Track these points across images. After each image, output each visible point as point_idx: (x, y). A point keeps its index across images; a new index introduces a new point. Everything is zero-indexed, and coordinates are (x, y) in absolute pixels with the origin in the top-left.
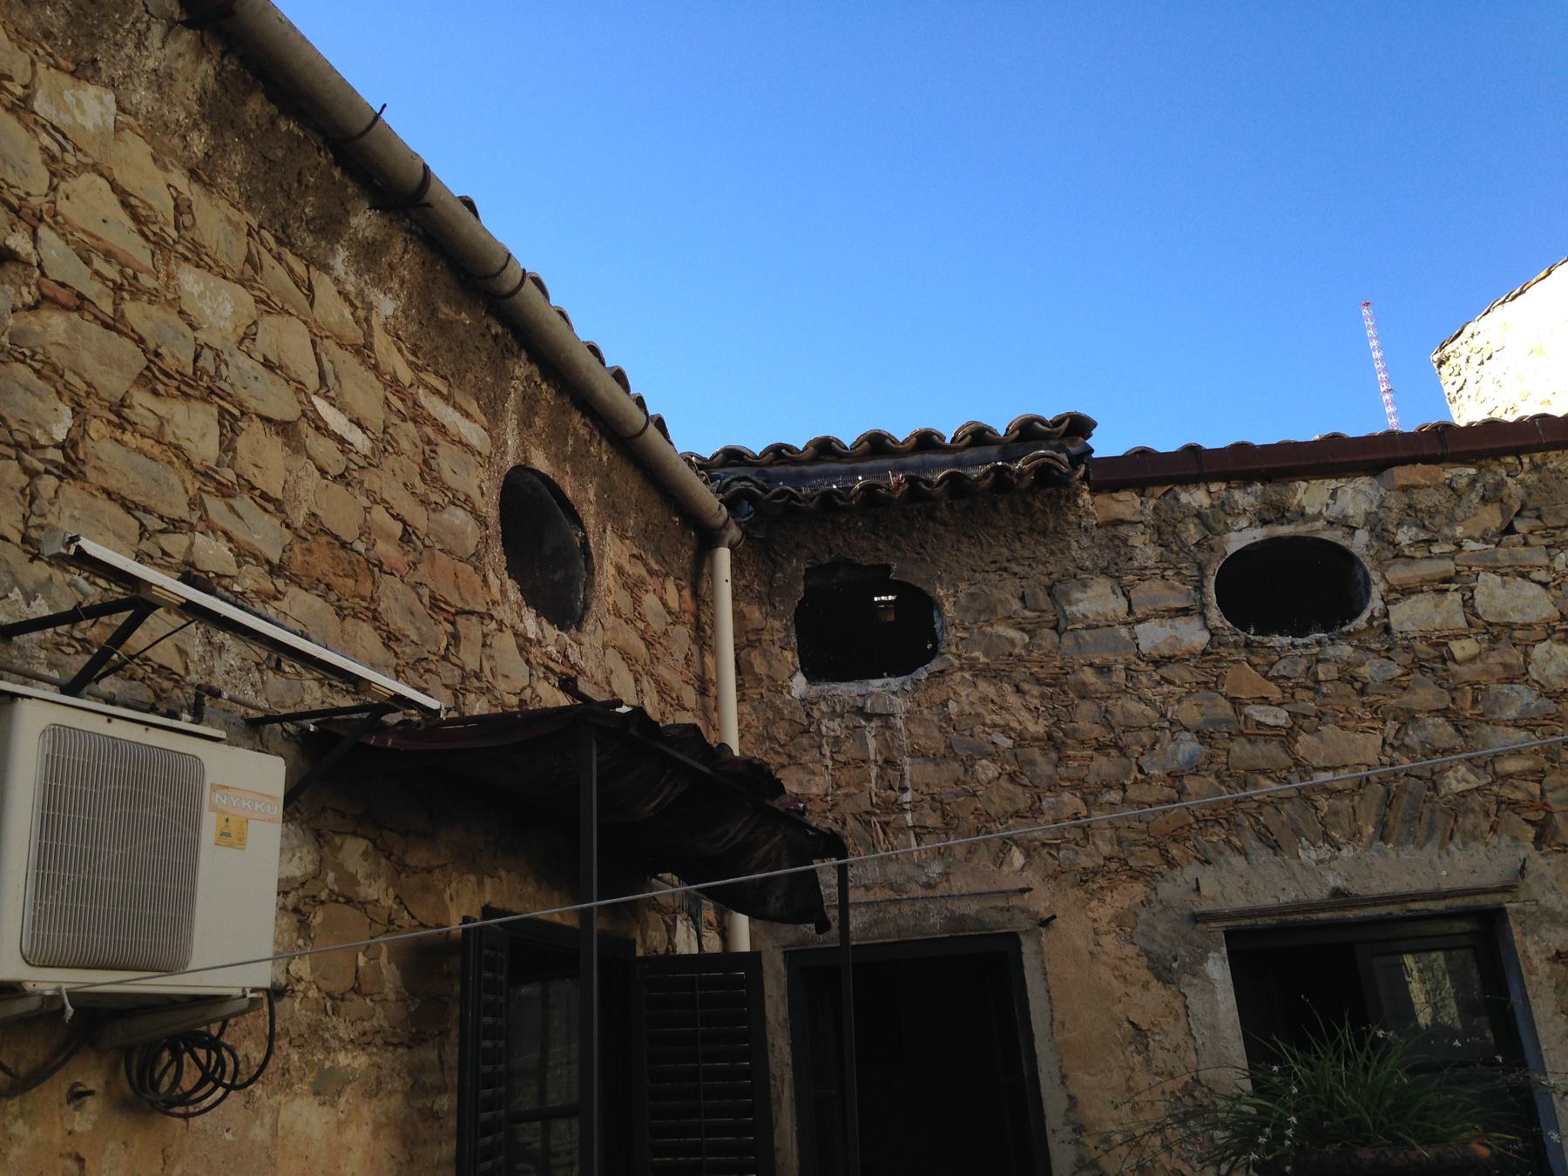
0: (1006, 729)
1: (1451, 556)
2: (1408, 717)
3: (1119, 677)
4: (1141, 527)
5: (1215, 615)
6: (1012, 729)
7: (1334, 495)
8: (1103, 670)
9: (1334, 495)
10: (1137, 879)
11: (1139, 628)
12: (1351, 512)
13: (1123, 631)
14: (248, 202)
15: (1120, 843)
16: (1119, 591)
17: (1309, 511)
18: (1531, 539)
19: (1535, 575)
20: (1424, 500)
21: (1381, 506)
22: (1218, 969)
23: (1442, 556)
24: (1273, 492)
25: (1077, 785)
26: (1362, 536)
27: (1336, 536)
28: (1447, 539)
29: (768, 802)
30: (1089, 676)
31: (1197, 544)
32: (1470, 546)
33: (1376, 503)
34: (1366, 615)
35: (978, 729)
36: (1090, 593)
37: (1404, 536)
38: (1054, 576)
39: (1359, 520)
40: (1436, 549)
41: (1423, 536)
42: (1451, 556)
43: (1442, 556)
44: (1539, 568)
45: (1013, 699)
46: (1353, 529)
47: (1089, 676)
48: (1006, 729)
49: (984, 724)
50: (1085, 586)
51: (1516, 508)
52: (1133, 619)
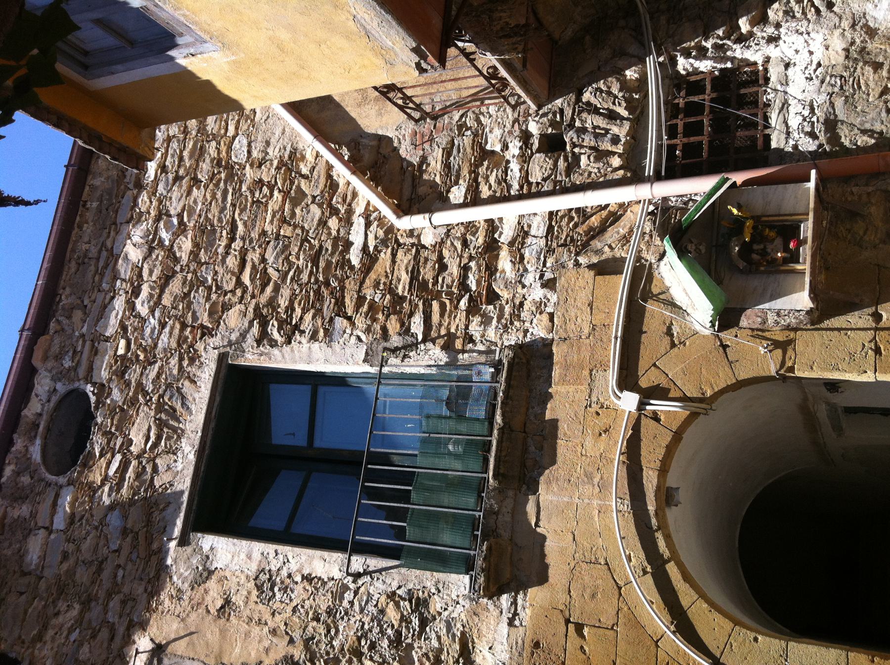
0: (71, 631)
1: (84, 342)
2: (140, 386)
3: (71, 547)
4: (9, 509)
5: (62, 480)
6: (72, 626)
7: (37, 396)
8: (65, 556)
9: (37, 396)
10: (160, 575)
11: (55, 527)
12: (47, 388)
13: (53, 536)
14: (134, 642)
15: (141, 579)
16: (37, 532)
17: (39, 411)
18: (93, 298)
19: (107, 301)
20: (55, 349)
21: (50, 371)
22: (208, 541)
23: (83, 346)
24: (22, 427)
25: (109, 595)
26: (59, 386)
27: (55, 399)
28: (77, 341)
29: (724, 28)
30: (65, 566)
31: (32, 478)
32: (84, 330)
33: (48, 374)
34: (91, 394)
35: (65, 650)
36: (31, 550)
37: (67, 363)
38: (17, 569)
39: (52, 384)
40: (79, 349)
41: (70, 354)
42: (84, 342)
43: (83, 346)
44: (105, 298)
45: (61, 619)
46: (55, 390)
47: (65, 566)
48: (71, 631)
49: (64, 644)
50: (27, 552)
51: (79, 302)
52: (49, 530)
